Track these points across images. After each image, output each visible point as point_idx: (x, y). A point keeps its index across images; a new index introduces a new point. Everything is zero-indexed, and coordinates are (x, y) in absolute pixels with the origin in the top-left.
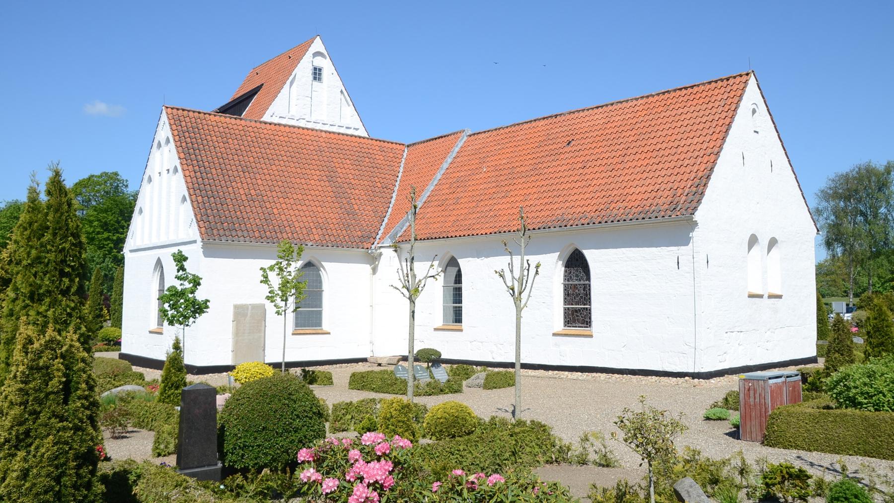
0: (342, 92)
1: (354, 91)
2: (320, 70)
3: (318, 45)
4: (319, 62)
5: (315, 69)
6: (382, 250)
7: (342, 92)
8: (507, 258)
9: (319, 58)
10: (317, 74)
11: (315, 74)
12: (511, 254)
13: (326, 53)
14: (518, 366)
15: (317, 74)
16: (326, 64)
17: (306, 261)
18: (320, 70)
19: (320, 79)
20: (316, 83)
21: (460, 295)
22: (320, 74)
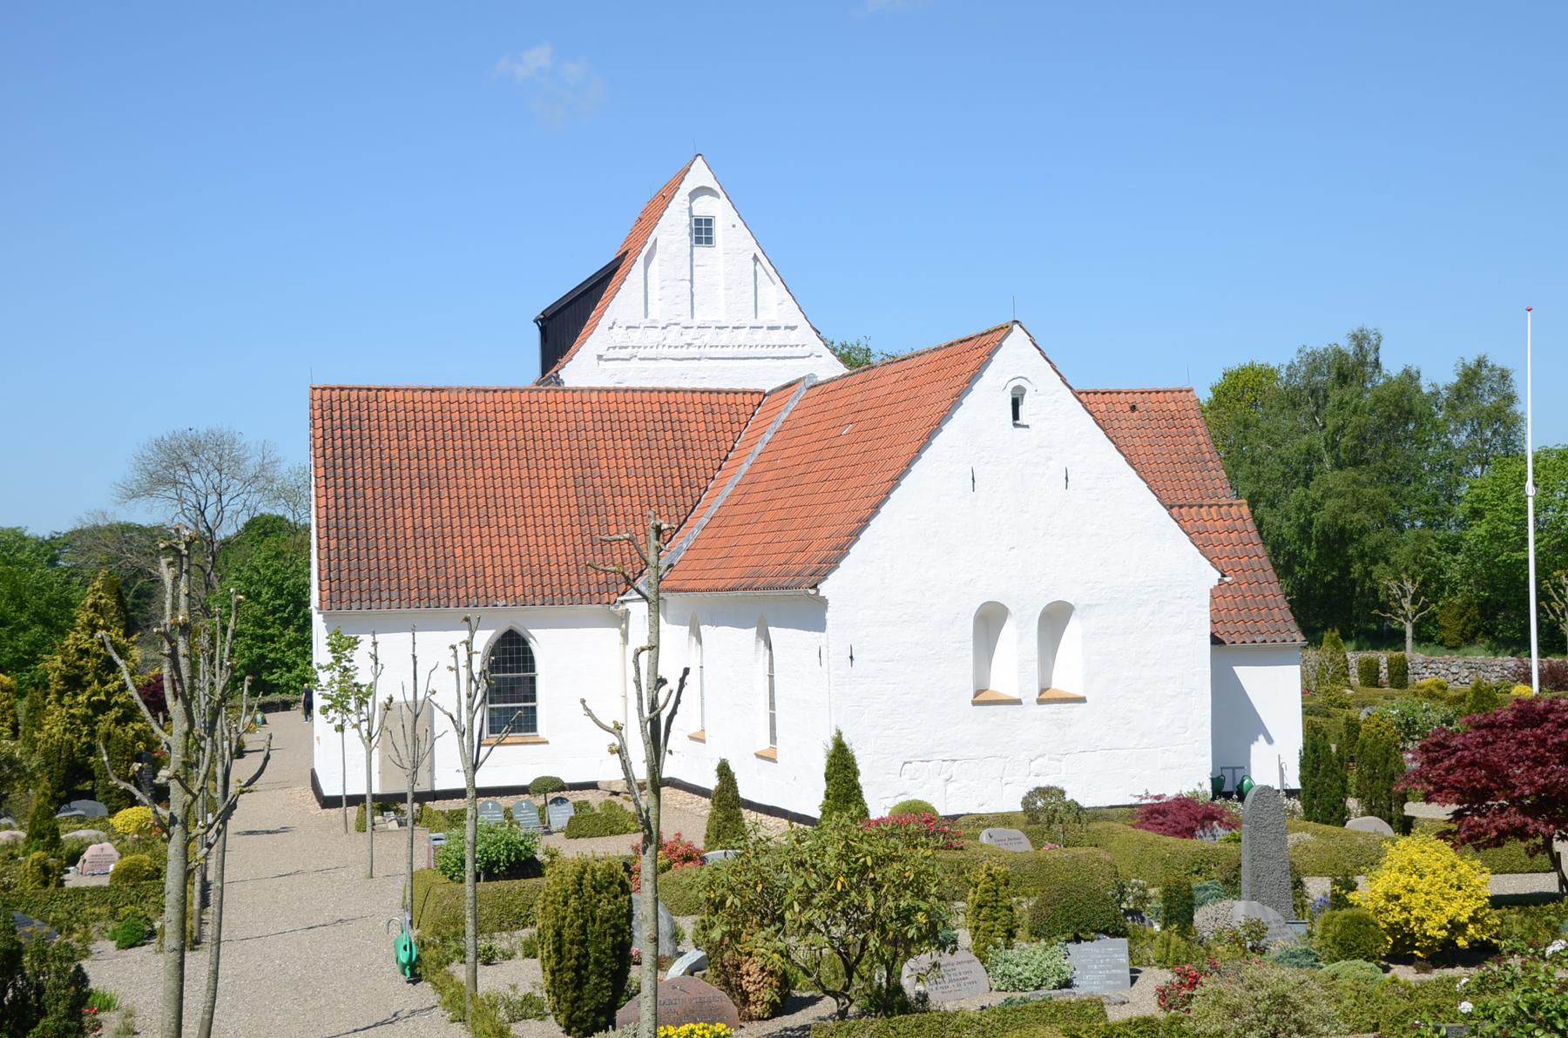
0: (755, 258)
1: (780, 255)
2: (709, 221)
3: (700, 174)
4: (704, 206)
5: (698, 221)
6: (628, 606)
7: (755, 258)
8: (465, 635)
9: (706, 198)
10: (702, 231)
11: (698, 231)
12: (413, 630)
13: (717, 188)
14: (470, 794)
15: (702, 231)
16: (717, 209)
17: (504, 629)
18: (709, 221)
19: (709, 241)
20: (700, 250)
21: (527, 690)
22: (709, 231)
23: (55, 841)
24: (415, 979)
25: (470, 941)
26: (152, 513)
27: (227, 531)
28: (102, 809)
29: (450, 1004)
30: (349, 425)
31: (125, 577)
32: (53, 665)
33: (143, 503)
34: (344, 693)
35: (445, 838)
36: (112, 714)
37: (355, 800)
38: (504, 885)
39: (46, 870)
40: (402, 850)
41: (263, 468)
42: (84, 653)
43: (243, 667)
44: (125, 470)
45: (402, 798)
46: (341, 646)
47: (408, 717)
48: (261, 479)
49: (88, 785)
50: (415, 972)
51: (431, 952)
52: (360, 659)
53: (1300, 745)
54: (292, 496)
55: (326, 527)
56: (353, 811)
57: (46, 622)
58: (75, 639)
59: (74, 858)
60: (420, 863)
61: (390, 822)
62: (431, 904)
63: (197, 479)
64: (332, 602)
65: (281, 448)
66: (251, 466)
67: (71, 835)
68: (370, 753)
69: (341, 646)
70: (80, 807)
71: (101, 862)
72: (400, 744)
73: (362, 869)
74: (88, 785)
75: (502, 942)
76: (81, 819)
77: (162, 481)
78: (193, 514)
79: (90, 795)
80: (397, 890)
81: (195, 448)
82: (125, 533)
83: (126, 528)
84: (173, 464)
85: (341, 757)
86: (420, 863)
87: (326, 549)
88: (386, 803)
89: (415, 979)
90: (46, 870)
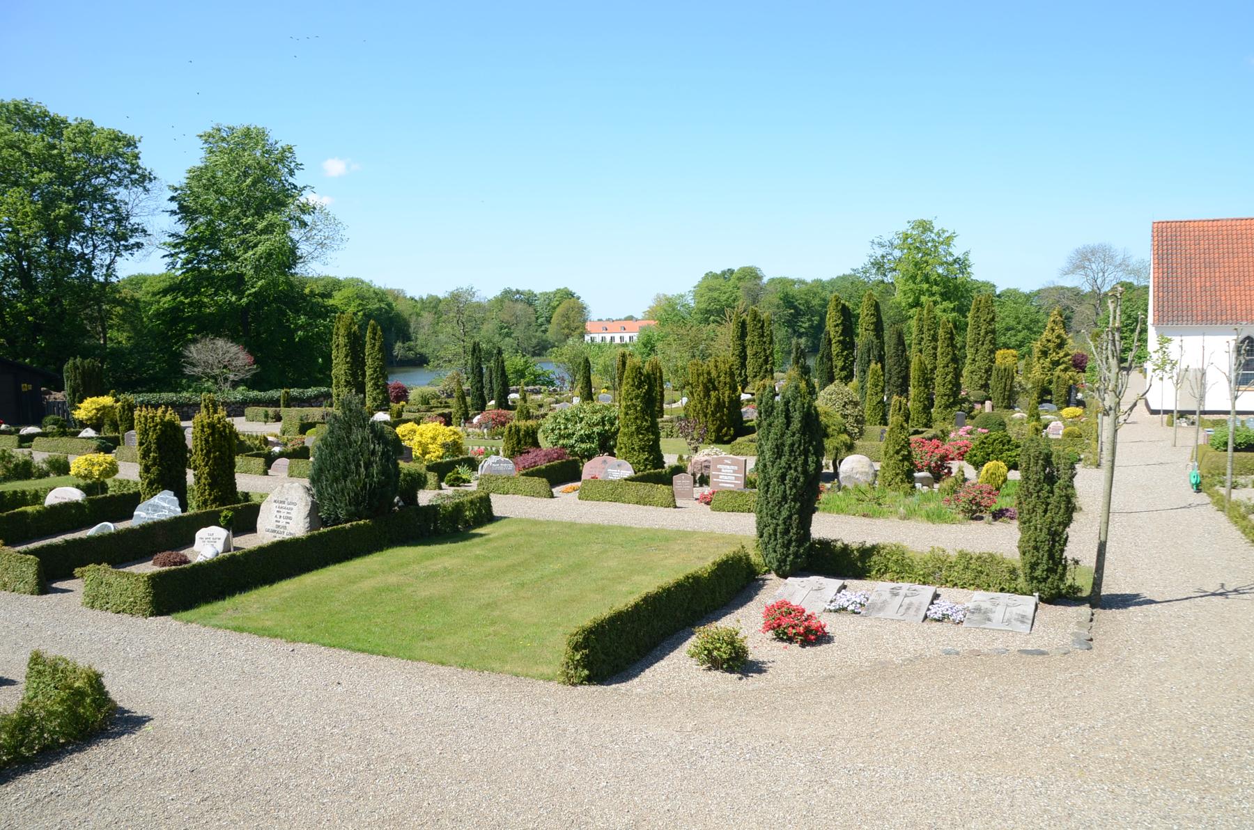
23: (1038, 419)
24: (1199, 490)
25: (1228, 477)
26: (1070, 282)
27: (1106, 289)
28: (1055, 408)
29: (1216, 503)
30: (1170, 240)
31: (1066, 308)
32: (1037, 346)
33: (1070, 277)
34: (1164, 363)
35: (1212, 431)
36: (1061, 367)
37: (1166, 412)
38: (1243, 454)
39: (1037, 430)
40: (1189, 436)
41: (1124, 260)
42: (1049, 341)
43: (68, 428)
44: (1063, 263)
45: (1193, 413)
46: (1164, 342)
47: (1199, 375)
48: (1124, 265)
49: (1049, 397)
50: (1198, 488)
51: (1207, 480)
52: (1173, 349)
53: (826, 277)
54: (1136, 272)
55: (1158, 287)
56: (1166, 417)
57: (1029, 329)
58: (1046, 334)
59: (1046, 427)
60: (1201, 442)
61: (1183, 423)
62: (1206, 459)
63: (1094, 266)
64: (1160, 321)
65: (1137, 252)
66: (1119, 259)
67: (1046, 417)
68: (900, 567)
69: (1164, 342)
70: (1046, 406)
71: (1058, 429)
72: (1195, 387)
73: (1170, 443)
74: (1049, 397)
75: (1241, 480)
76: (1047, 411)
77: (1078, 267)
78: (1091, 281)
79: (1050, 402)
80: (1187, 453)
81: (1093, 252)
82: (1061, 290)
83: (1062, 288)
84: (1083, 259)
85: (1164, 395)
86: (1201, 442)
87: (1157, 297)
88: (1182, 414)
89: (1199, 490)
90: (1037, 430)
